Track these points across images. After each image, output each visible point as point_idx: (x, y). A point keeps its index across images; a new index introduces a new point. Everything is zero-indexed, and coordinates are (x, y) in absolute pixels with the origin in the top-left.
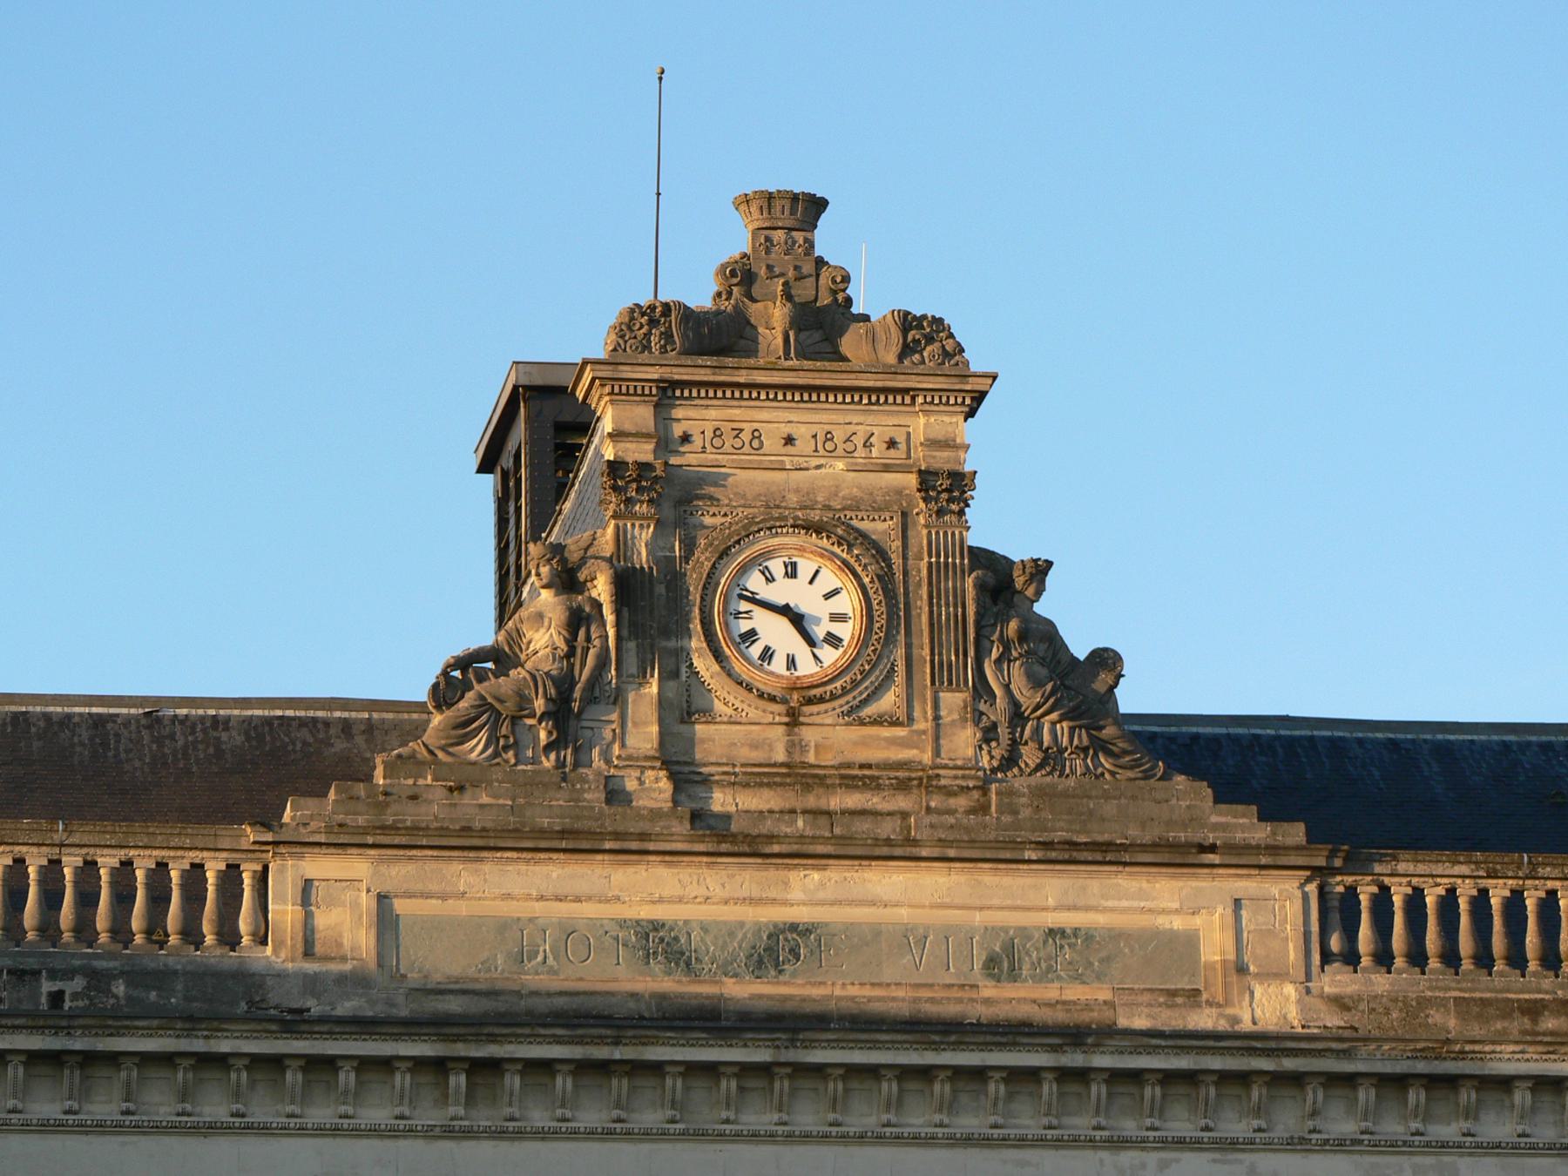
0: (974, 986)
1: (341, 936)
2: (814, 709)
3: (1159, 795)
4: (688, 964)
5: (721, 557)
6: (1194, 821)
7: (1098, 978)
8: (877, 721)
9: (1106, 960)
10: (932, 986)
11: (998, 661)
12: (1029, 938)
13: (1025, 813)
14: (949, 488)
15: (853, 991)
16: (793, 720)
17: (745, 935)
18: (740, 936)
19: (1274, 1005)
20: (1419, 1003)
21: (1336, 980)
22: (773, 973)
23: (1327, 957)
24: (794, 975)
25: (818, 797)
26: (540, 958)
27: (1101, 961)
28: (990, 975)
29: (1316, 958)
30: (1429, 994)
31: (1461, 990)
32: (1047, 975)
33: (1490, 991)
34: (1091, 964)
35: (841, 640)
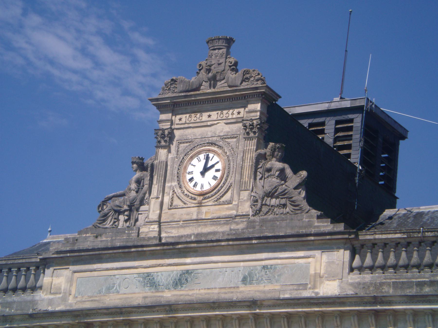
0: (238, 287)
1: (61, 286)
2: (206, 201)
3: (299, 218)
4: (156, 286)
5: (185, 155)
6: (310, 225)
7: (276, 282)
8: (224, 203)
9: (279, 276)
10: (225, 288)
11: (261, 179)
12: (257, 269)
13: (257, 228)
15: (202, 291)
17: (173, 275)
18: (172, 276)
20: (380, 284)
21: (355, 277)
22: (180, 287)
24: (186, 287)
25: (202, 229)
26: (115, 288)
27: (278, 276)
28: (243, 283)
29: (347, 270)
30: (385, 281)
31: (396, 279)
32: (259, 282)
33: (406, 278)
34: (275, 277)
35: (217, 177)
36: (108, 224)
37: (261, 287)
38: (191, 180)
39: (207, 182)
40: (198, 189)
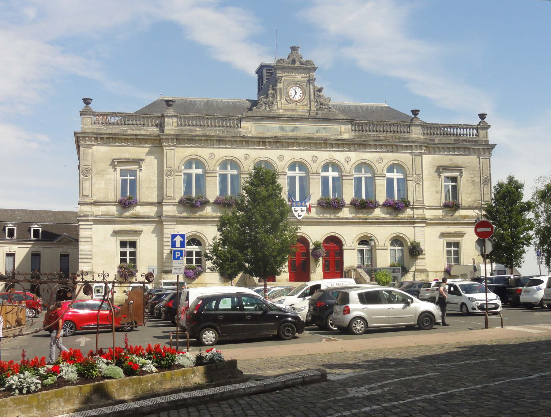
14: (310, 81)
16: (296, 105)
19: (346, 136)
39: (297, 97)
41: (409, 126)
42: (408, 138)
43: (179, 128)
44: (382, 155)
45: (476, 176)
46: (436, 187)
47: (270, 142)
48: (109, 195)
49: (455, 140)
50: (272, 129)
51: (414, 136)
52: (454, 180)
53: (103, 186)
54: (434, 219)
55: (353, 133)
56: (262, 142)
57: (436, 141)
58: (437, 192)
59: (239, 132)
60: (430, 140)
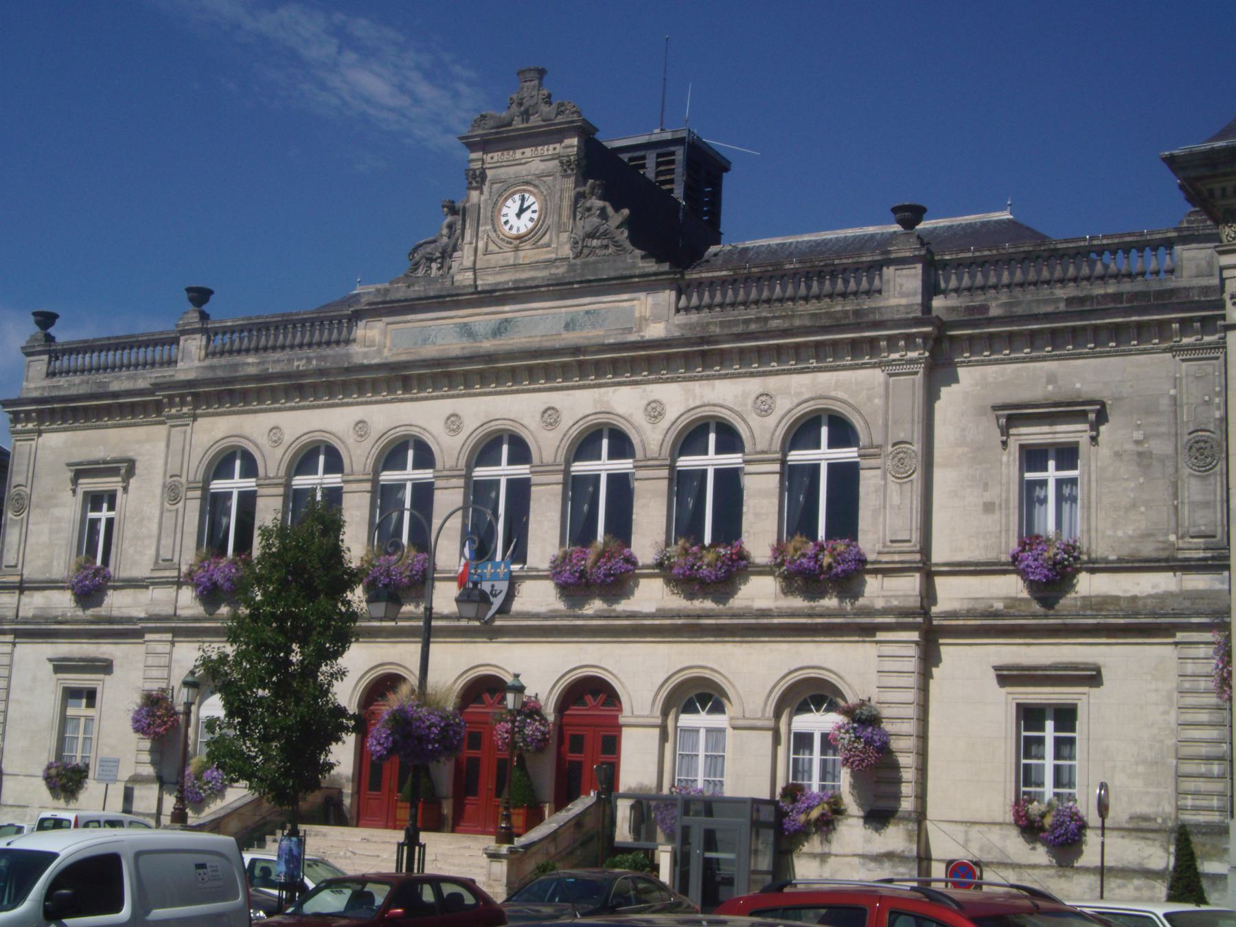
8: (542, 246)
19: (656, 331)
23: (678, 310)
36: (421, 272)
37: (585, 333)
38: (506, 223)
39: (523, 225)
40: (514, 232)
41: (876, 267)
42: (873, 310)
43: (207, 363)
44: (772, 383)
45: (1158, 436)
46: (986, 487)
47: (421, 378)
48: (55, 563)
49: (1070, 301)
50: (440, 334)
51: (893, 302)
52: (1067, 455)
53: (44, 538)
54: (970, 614)
55: (681, 318)
56: (402, 378)
57: (994, 312)
58: (988, 508)
59: (348, 356)
60: (970, 310)
